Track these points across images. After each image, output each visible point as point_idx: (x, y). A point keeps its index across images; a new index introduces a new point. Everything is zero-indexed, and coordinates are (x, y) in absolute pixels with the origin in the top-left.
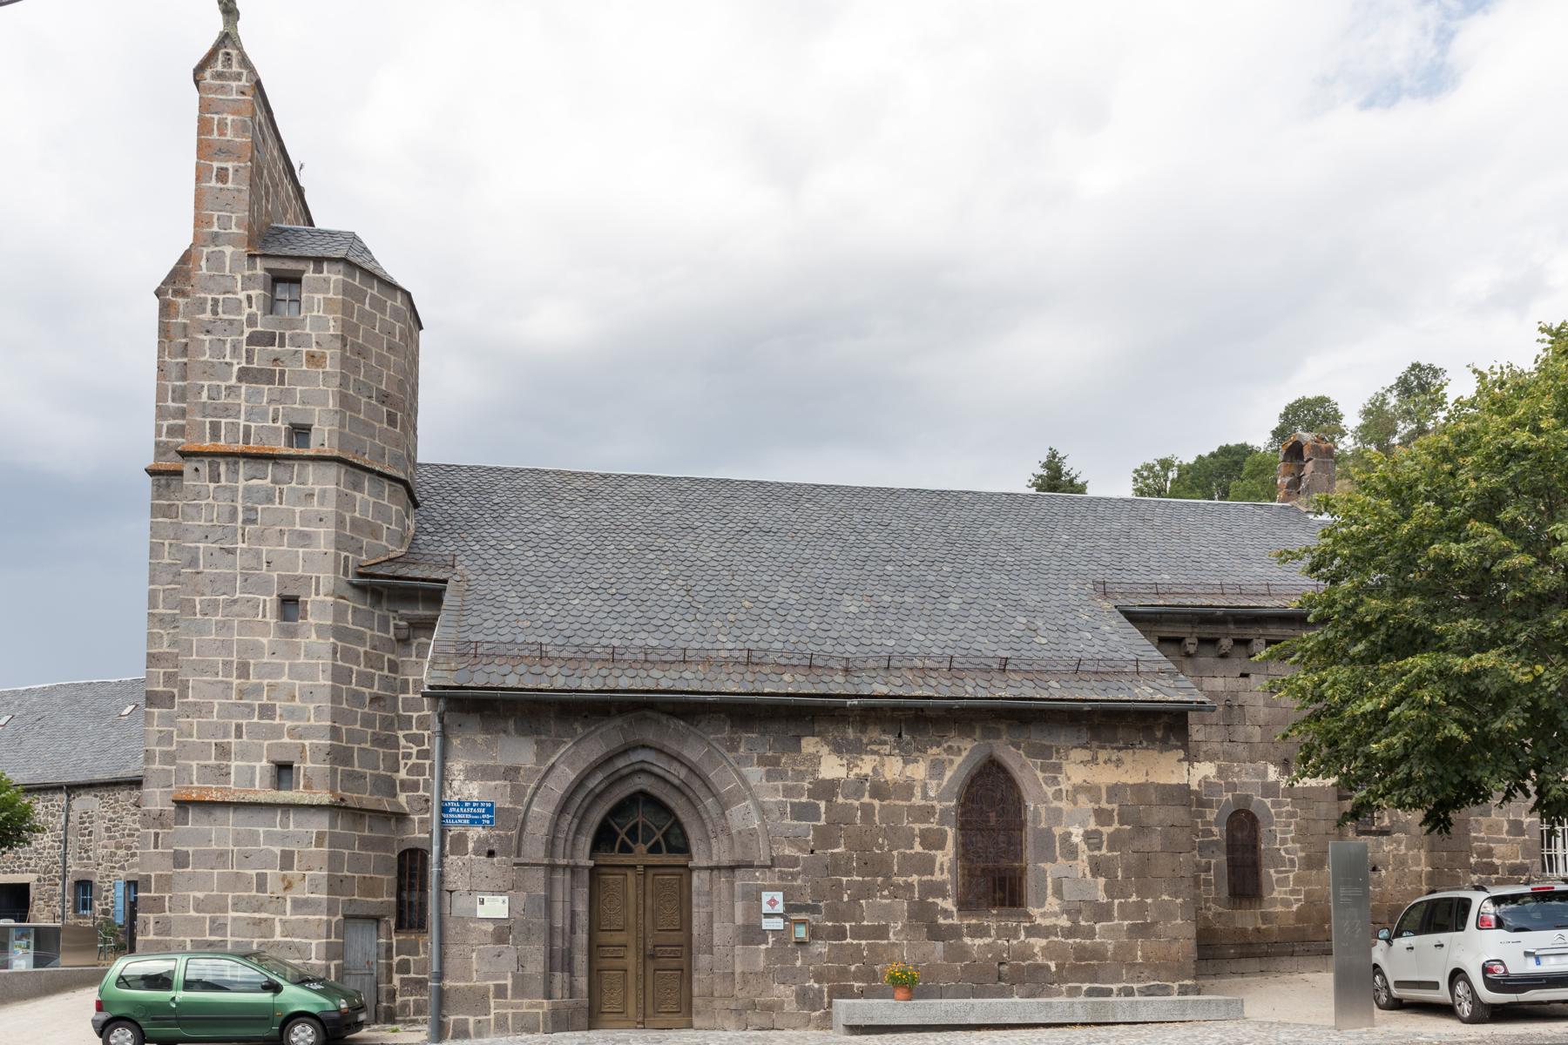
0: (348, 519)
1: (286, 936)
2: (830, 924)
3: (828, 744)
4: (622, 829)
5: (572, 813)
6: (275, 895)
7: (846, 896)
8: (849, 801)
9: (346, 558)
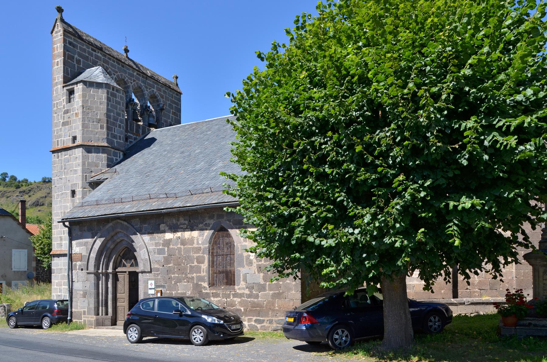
8: (174, 247)
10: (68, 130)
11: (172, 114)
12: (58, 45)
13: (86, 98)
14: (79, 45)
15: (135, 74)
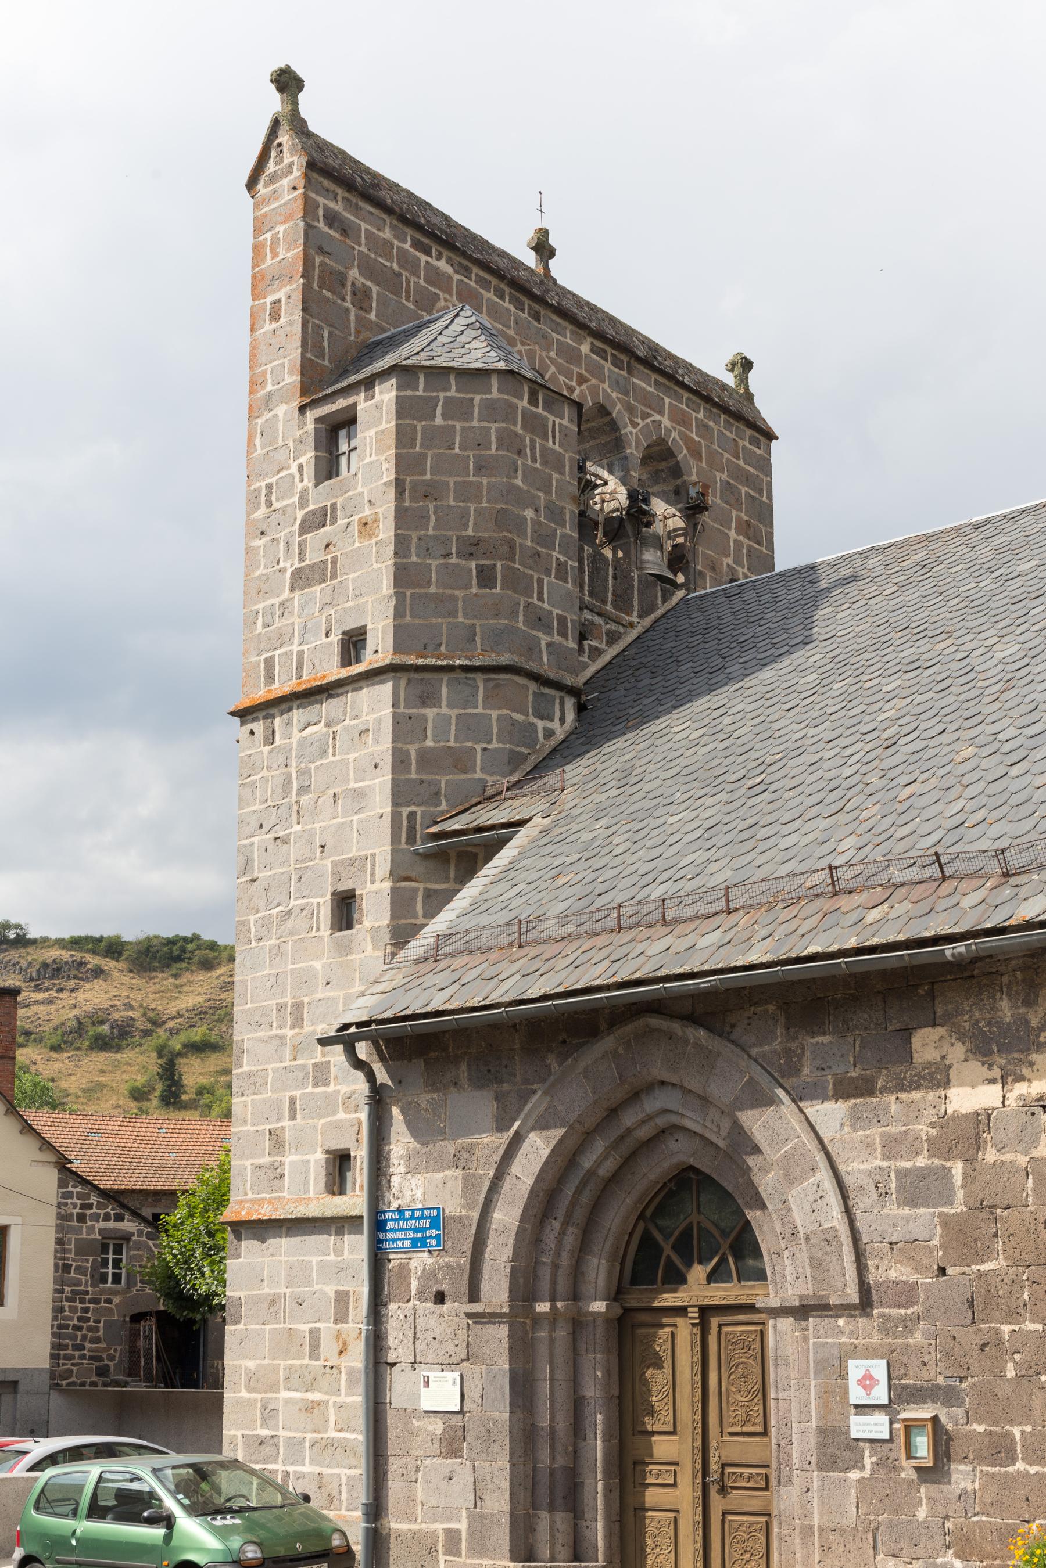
0: (413, 754)
1: (341, 1430)
2: (981, 1429)
3: (962, 1038)
4: (667, 1237)
5: (561, 1218)
6: (329, 1364)
7: (1010, 1366)
8: (1008, 1157)
9: (412, 816)
10: (323, 606)
11: (738, 532)
12: (281, 229)
13: (413, 445)
14: (364, 226)
15: (585, 348)
